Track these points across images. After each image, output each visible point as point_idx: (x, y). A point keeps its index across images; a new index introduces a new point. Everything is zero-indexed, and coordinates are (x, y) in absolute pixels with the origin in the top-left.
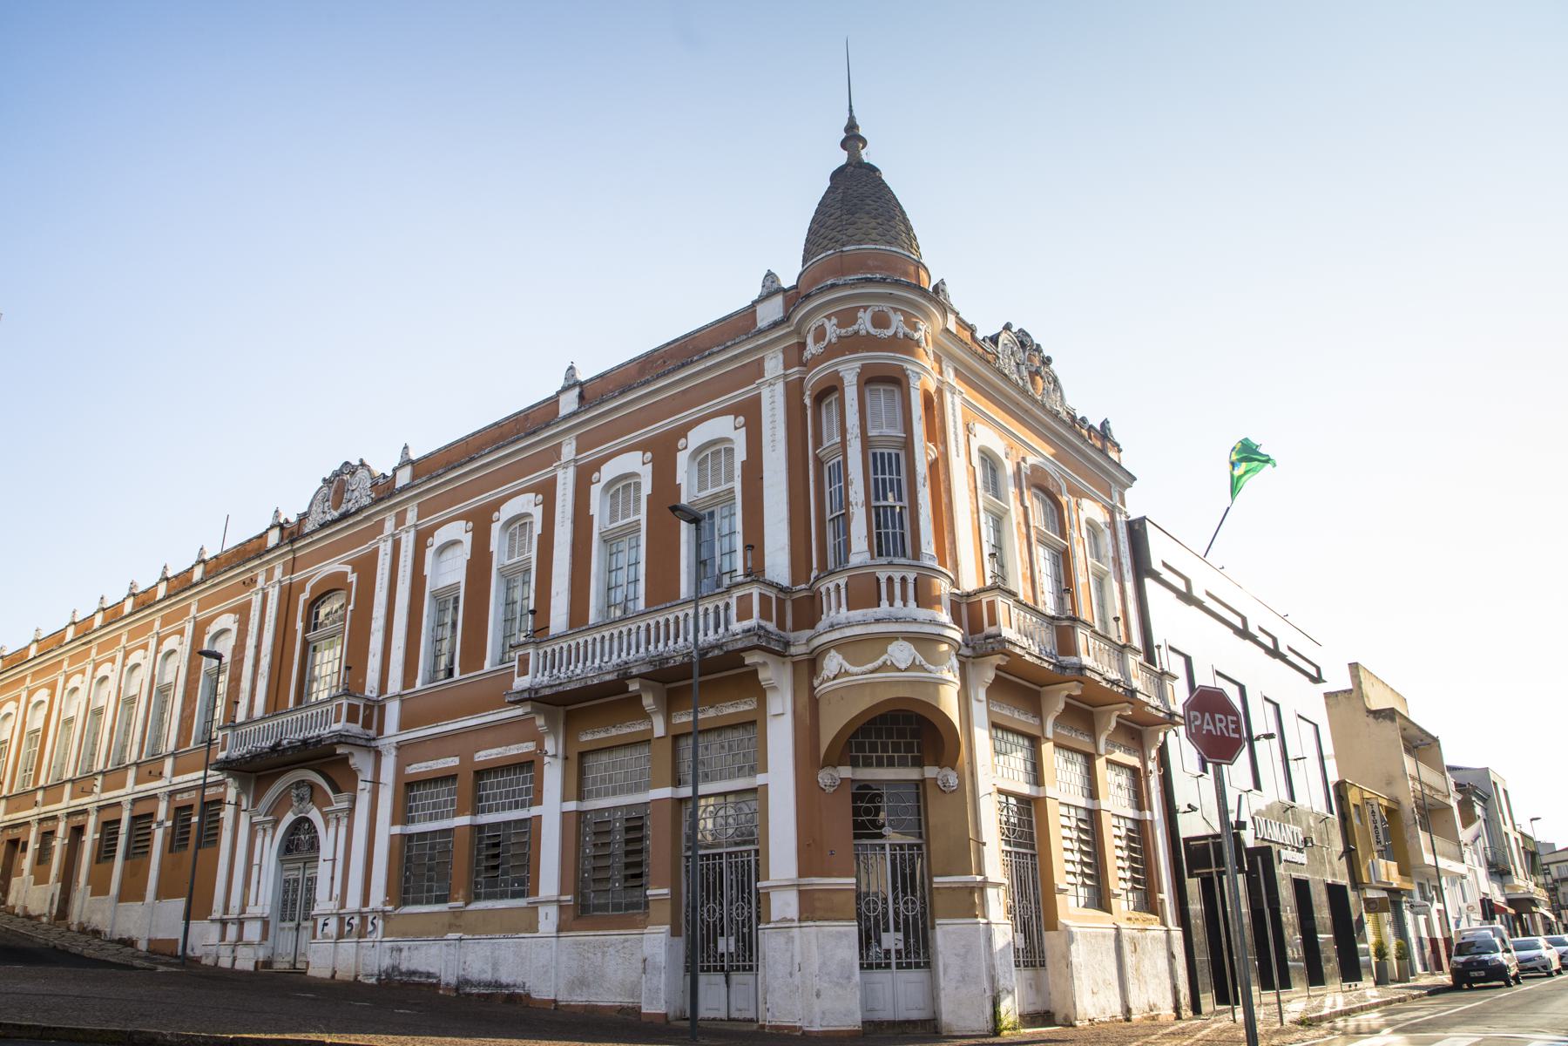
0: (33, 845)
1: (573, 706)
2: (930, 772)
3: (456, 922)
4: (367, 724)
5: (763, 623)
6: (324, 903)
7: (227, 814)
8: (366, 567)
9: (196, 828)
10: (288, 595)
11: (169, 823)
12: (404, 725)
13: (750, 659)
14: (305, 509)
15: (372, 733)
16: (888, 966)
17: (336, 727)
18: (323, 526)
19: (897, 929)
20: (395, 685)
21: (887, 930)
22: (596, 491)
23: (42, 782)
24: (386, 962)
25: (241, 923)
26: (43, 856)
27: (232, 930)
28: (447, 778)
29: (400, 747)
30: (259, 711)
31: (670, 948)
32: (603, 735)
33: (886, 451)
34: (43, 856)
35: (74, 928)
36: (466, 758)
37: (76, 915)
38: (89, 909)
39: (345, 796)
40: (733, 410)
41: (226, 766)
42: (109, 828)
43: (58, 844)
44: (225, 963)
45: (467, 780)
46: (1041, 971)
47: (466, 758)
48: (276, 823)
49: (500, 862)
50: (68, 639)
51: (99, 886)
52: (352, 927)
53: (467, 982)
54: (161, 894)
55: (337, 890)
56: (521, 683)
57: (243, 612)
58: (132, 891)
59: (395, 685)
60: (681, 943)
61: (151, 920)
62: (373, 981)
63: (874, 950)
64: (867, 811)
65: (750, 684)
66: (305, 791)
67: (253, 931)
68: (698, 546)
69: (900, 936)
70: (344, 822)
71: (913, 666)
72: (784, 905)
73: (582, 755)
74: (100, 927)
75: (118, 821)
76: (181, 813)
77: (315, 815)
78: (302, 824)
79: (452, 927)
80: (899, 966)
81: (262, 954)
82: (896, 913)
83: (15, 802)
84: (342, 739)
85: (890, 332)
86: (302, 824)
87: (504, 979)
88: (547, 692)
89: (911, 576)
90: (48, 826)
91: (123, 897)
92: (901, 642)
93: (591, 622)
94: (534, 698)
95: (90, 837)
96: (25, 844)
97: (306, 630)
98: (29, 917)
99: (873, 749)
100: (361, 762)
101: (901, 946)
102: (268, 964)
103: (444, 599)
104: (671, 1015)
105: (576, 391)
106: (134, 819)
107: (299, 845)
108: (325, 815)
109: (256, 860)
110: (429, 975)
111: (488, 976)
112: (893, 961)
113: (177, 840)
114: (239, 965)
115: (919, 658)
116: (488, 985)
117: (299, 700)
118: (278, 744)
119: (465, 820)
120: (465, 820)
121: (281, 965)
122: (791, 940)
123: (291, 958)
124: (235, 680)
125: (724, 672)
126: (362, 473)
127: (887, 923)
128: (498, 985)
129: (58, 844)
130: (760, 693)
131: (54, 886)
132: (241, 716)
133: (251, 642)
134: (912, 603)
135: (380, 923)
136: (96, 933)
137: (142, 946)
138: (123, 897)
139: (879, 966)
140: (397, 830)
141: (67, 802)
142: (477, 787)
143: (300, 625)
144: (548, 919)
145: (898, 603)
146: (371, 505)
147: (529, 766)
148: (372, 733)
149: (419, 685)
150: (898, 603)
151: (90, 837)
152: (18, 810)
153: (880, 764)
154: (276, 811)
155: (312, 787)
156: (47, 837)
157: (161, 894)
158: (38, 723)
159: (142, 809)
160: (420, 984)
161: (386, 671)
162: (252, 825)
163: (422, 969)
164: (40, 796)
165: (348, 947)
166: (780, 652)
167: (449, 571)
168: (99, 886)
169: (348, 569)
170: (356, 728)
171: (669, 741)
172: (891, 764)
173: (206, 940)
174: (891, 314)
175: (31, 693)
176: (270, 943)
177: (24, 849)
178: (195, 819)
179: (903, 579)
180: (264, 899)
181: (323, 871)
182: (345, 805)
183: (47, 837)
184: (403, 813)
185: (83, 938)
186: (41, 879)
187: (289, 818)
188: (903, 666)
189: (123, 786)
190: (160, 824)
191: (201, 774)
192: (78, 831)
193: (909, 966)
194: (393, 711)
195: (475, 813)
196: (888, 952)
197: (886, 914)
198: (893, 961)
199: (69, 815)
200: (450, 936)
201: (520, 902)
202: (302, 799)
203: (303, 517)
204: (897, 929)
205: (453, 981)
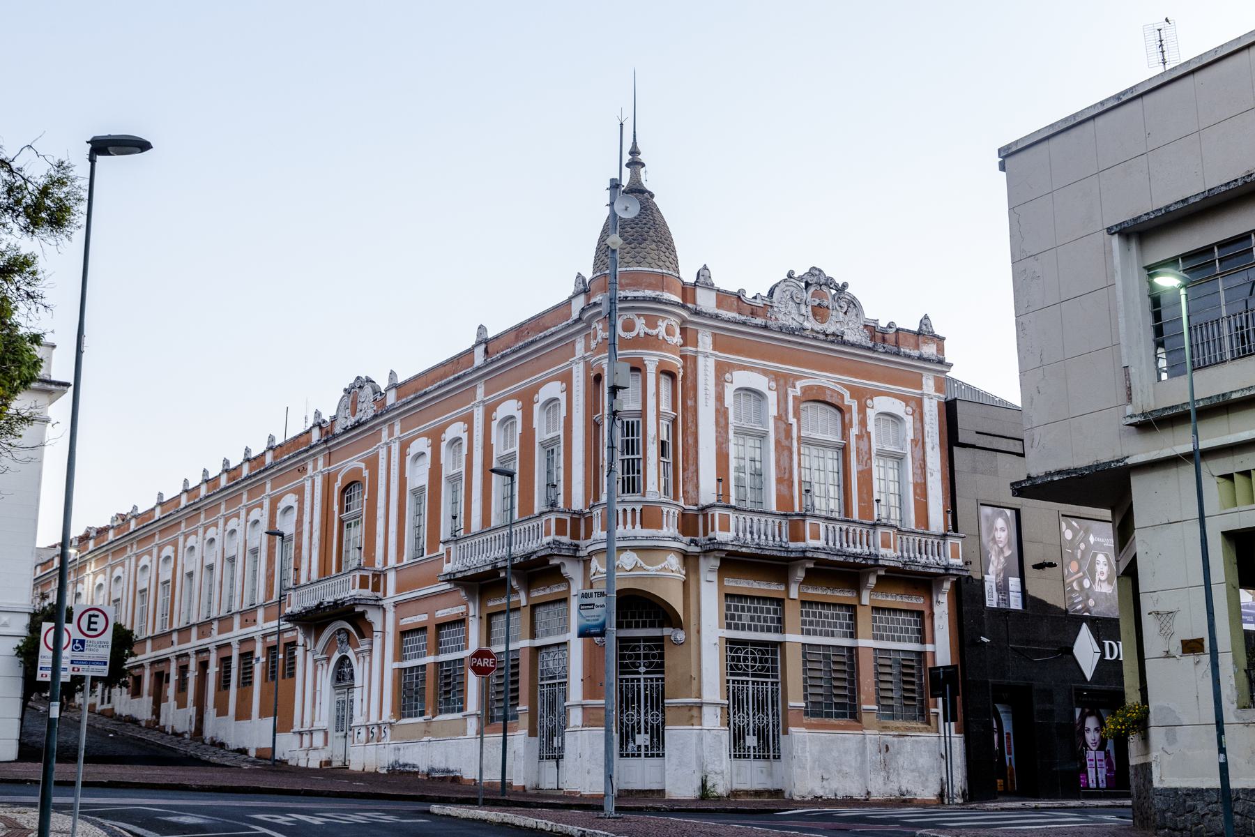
0: (174, 677)
1: (482, 585)
2: (667, 631)
3: (428, 729)
4: (376, 588)
5: (558, 538)
6: (358, 720)
7: (299, 652)
8: (372, 463)
9: (281, 664)
10: (328, 480)
11: (264, 660)
12: (399, 590)
13: (554, 562)
14: (334, 413)
15: (380, 594)
16: (639, 755)
17: (353, 592)
18: (346, 431)
19: (646, 732)
20: (392, 561)
21: (639, 733)
22: (494, 424)
23: (175, 626)
24: (392, 759)
25: (311, 733)
26: (182, 686)
27: (306, 738)
28: (423, 629)
29: (396, 605)
30: (314, 576)
31: (527, 745)
32: (542, 593)
33: (630, 420)
34: (182, 686)
35: (207, 741)
36: (431, 615)
37: (209, 732)
38: (215, 727)
39: (366, 640)
40: (906, 399)
41: (291, 618)
42: (905, 682)
43: (192, 675)
44: (303, 764)
45: (432, 630)
46: (776, 764)
47: (431, 615)
48: (329, 659)
49: (448, 690)
50: (182, 506)
51: (222, 710)
52: (374, 733)
53: (433, 770)
54: (263, 714)
55: (365, 709)
56: (447, 568)
57: (300, 491)
58: (243, 714)
59: (392, 561)
60: (536, 741)
61: (254, 734)
62: (384, 771)
63: (631, 745)
64: (654, 656)
65: (555, 575)
66: (343, 636)
67: (318, 739)
68: (549, 472)
69: (648, 736)
70: (368, 659)
71: (635, 567)
72: (576, 717)
73: (490, 616)
74: (224, 740)
75: (230, 658)
76: (271, 650)
77: (351, 654)
78: (343, 660)
79: (426, 733)
80: (646, 755)
81: (324, 756)
82: (646, 723)
83: (158, 642)
84: (357, 601)
85: (634, 334)
86: (343, 660)
87: (451, 768)
88: (459, 575)
89: (638, 508)
90: (183, 661)
91: (239, 717)
92: (629, 552)
93: (493, 525)
94: (452, 579)
95: (213, 670)
96: (168, 675)
97: (341, 512)
98: (175, 734)
99: (633, 617)
100: (373, 616)
101: (648, 743)
102: (329, 763)
103: (418, 492)
104: (528, 786)
105: (483, 346)
106: (242, 655)
107: (343, 676)
108: (356, 654)
109: (318, 688)
110: (414, 766)
111: (443, 766)
112: (643, 752)
113: (271, 673)
114: (311, 765)
115: (640, 561)
116: (443, 771)
117: (339, 569)
118: (321, 603)
119: (430, 659)
120: (430, 659)
121: (337, 763)
122: (576, 738)
123: (342, 758)
124: (299, 548)
125: (538, 571)
126: (368, 389)
127: (639, 729)
128: (449, 771)
129: (192, 675)
130: (566, 581)
131: (191, 710)
132: (303, 581)
133: (306, 519)
134: (638, 525)
135: (388, 731)
136: (222, 745)
137: (252, 753)
138: (239, 717)
139: (633, 755)
140: (397, 665)
141: (195, 642)
142: (438, 636)
143: (336, 508)
144: (472, 725)
145: (629, 526)
146: (375, 417)
147: (461, 622)
148: (380, 594)
149: (405, 561)
150: (629, 526)
151: (213, 670)
152: (160, 648)
153: (637, 626)
154: (329, 649)
155: (348, 632)
156: (183, 670)
157: (263, 714)
158: (169, 576)
159: (246, 649)
160: (410, 772)
161: (386, 554)
162: (315, 661)
163: (410, 762)
164: (175, 637)
165: (371, 747)
166: (573, 553)
167: (419, 476)
168: (222, 710)
169: (363, 465)
170: (367, 593)
171: (528, 609)
172: (644, 626)
173: (289, 748)
174: (636, 319)
175: (160, 549)
176: (329, 747)
177: (168, 681)
178: (281, 656)
179: (634, 510)
180: (325, 716)
181: (357, 694)
182: (367, 647)
183: (183, 670)
184: (400, 655)
185: (213, 749)
186: (182, 704)
187: (336, 656)
188: (628, 568)
189: (231, 630)
190: (258, 659)
191: (275, 623)
192: (204, 666)
193: (652, 755)
194: (391, 577)
195: (437, 654)
196: (639, 747)
197: (639, 723)
198: (643, 752)
199: (152, 664)
200: (426, 739)
201: (459, 715)
202: (342, 642)
203: (334, 419)
204: (646, 732)
205: (426, 770)
